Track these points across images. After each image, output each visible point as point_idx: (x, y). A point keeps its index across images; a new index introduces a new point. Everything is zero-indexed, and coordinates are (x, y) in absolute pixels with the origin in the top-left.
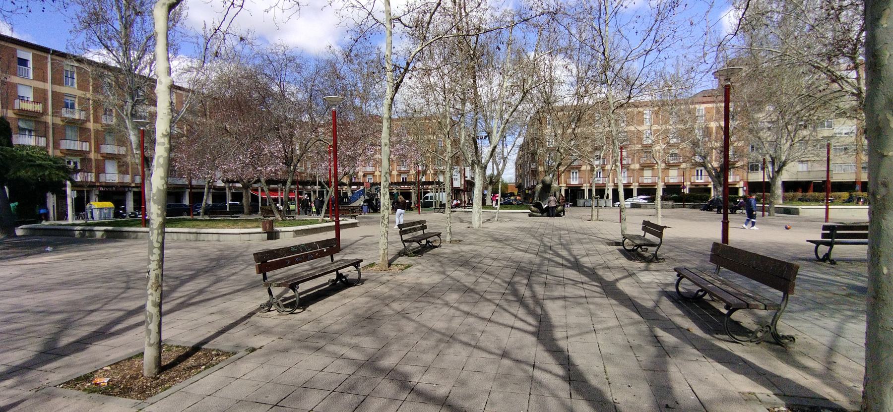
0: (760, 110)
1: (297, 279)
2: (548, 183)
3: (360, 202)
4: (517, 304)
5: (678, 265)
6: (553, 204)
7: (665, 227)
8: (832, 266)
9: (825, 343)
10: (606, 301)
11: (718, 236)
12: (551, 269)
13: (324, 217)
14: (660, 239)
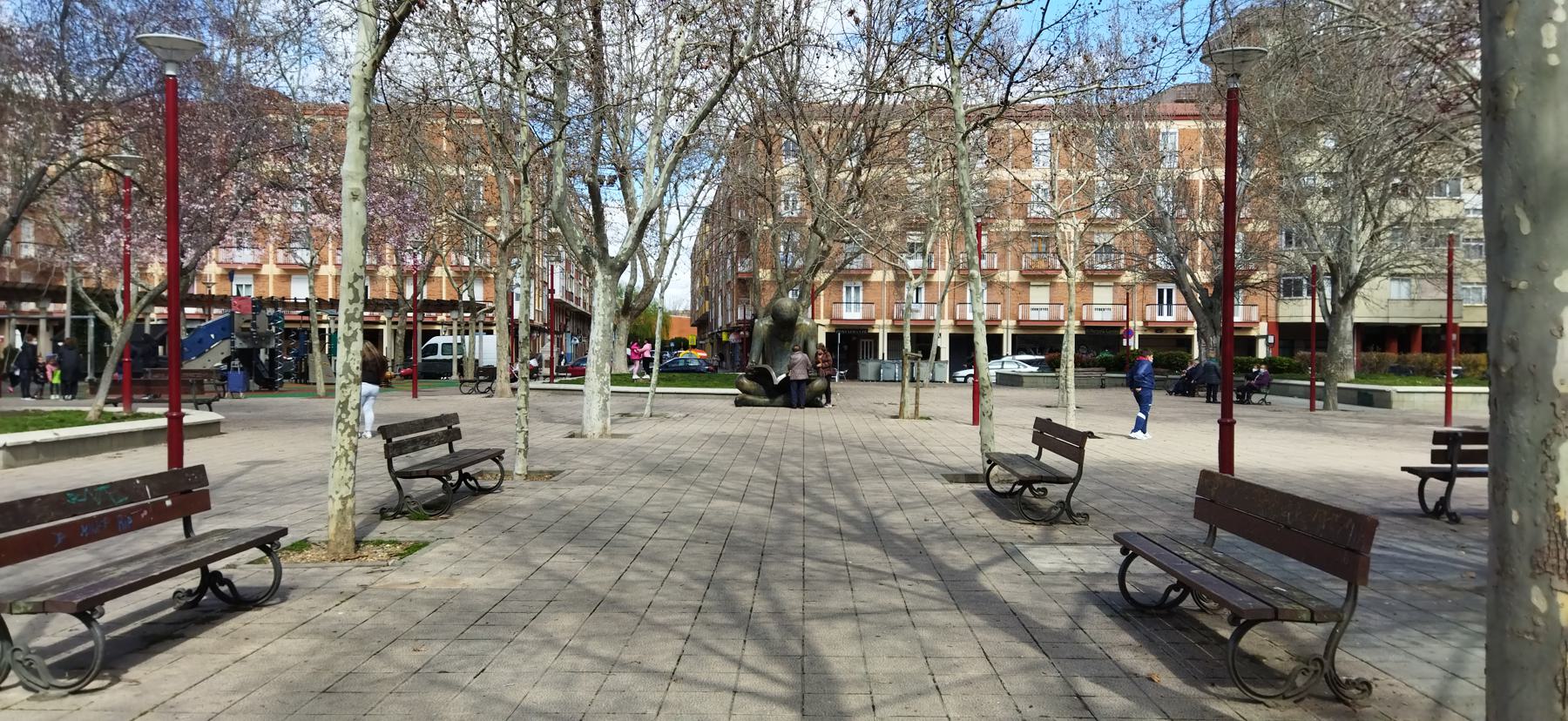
0: (1309, 143)
1: (95, 587)
2: (787, 315)
3: (214, 358)
4: (739, 634)
5: (1120, 529)
6: (801, 374)
7: (1091, 435)
8: (1452, 527)
9: (1430, 692)
10: (954, 618)
11: (1210, 458)
12: (813, 543)
13: (107, 403)
14: (1075, 465)
